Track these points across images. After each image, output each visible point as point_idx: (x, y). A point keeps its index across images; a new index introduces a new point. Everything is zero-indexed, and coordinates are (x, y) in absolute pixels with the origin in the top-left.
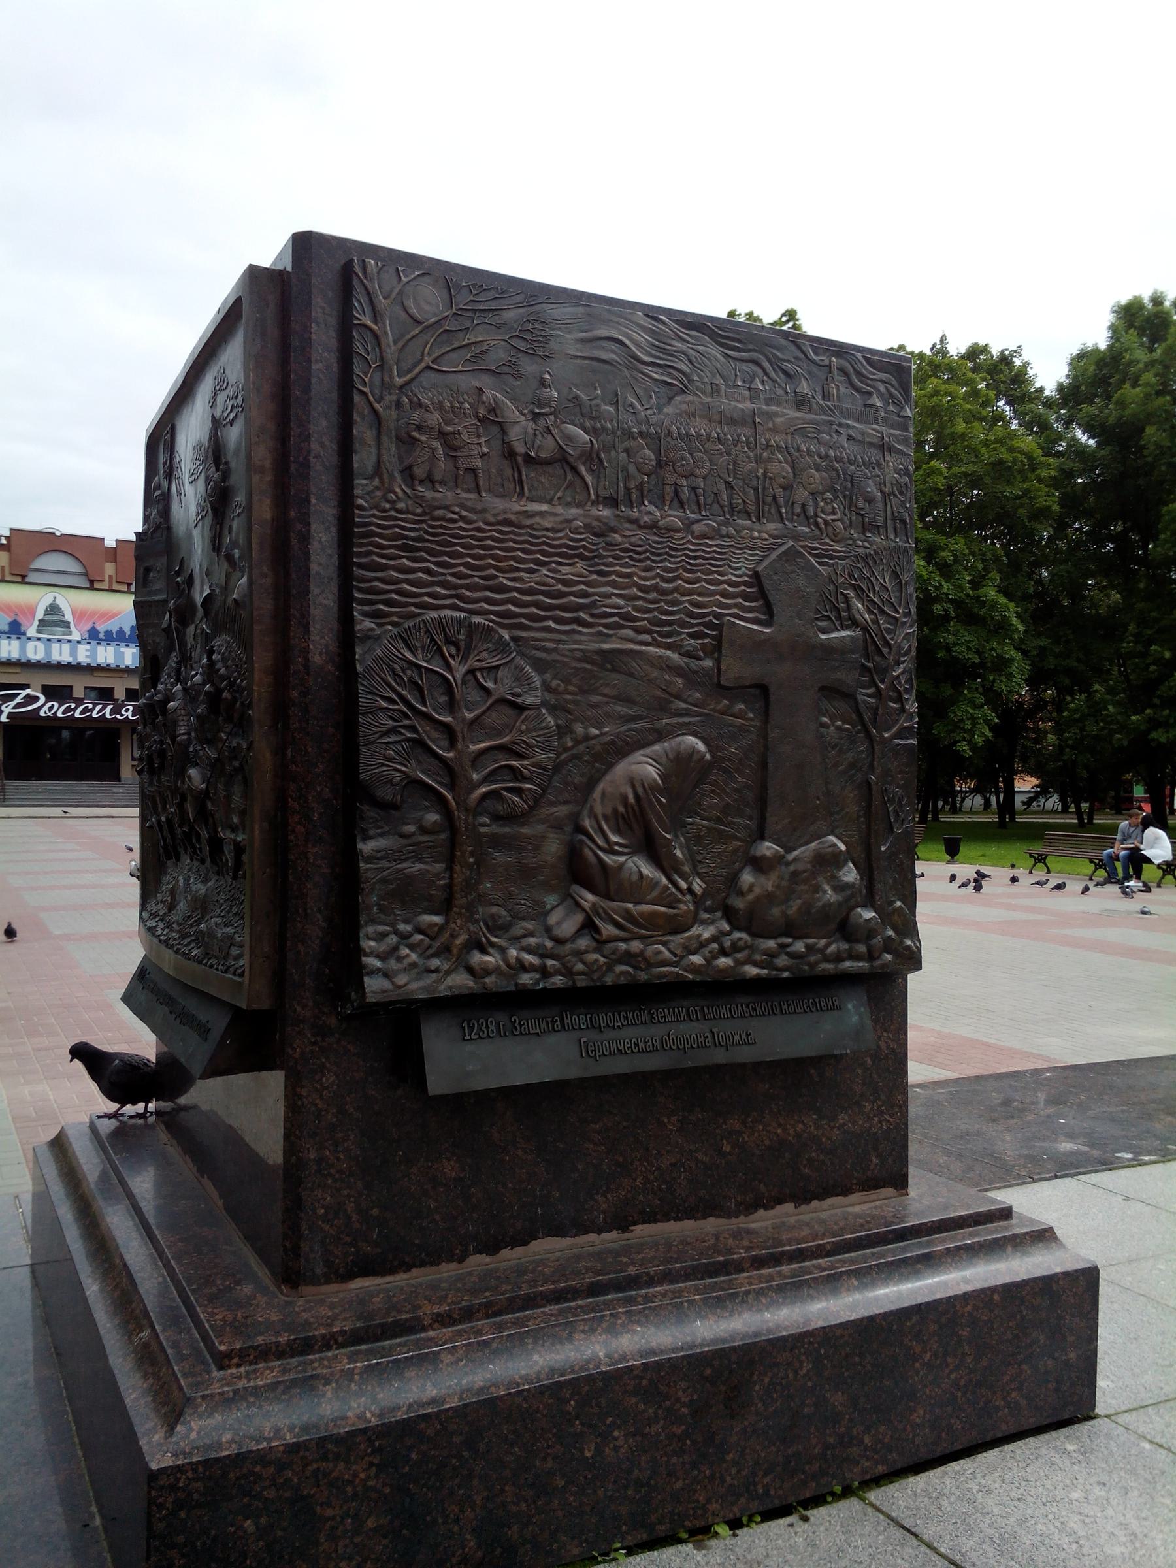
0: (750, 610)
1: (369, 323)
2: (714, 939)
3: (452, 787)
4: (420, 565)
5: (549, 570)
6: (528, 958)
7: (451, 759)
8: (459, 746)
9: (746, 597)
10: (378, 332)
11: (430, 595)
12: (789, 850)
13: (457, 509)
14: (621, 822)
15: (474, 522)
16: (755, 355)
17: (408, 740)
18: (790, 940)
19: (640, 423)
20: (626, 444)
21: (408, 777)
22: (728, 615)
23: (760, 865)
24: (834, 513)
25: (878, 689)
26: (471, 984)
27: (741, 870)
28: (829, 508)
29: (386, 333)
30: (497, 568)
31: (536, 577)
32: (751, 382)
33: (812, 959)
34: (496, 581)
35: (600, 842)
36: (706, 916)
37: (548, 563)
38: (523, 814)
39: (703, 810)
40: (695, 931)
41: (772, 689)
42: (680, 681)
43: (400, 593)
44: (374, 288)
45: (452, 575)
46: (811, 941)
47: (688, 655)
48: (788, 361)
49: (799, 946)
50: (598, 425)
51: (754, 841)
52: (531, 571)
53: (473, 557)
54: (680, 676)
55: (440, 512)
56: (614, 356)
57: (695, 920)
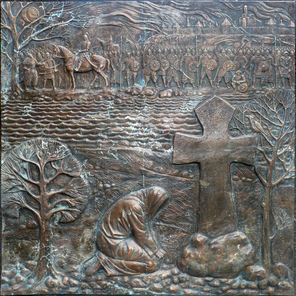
0: (191, 128)
1: (8, 27)
2: (168, 277)
3: (39, 210)
4: (28, 120)
5: (86, 117)
6: (75, 282)
7: (38, 199)
8: (42, 194)
9: (189, 122)
10: (11, 30)
11: (32, 131)
12: (212, 238)
13: (43, 96)
14: (119, 225)
15: (51, 100)
16: (197, 12)
17: (21, 191)
18: (212, 278)
19: (132, 49)
20: (282, 125)
21: (21, 206)
22: (178, 131)
23: (195, 245)
24: (242, 79)
25: (268, 162)
26: (46, 291)
27: (186, 246)
28: (239, 77)
29: (14, 29)
30: (60, 118)
31: (79, 121)
32: (196, 24)
33: (224, 288)
34: (61, 124)
35: (109, 235)
36: (165, 266)
37: (85, 114)
38: (73, 221)
39: (166, 219)
40: (159, 273)
41: (203, 164)
42: (151, 162)
43: (20, 131)
44: (9, 13)
45: (42, 122)
46: (223, 280)
47: (155, 150)
48: (218, 12)
49: (216, 283)
50: (111, 53)
51: (194, 233)
52: (76, 118)
53: (51, 115)
54: (152, 160)
55: (36, 98)
56: (120, 23)
57: (159, 267)
